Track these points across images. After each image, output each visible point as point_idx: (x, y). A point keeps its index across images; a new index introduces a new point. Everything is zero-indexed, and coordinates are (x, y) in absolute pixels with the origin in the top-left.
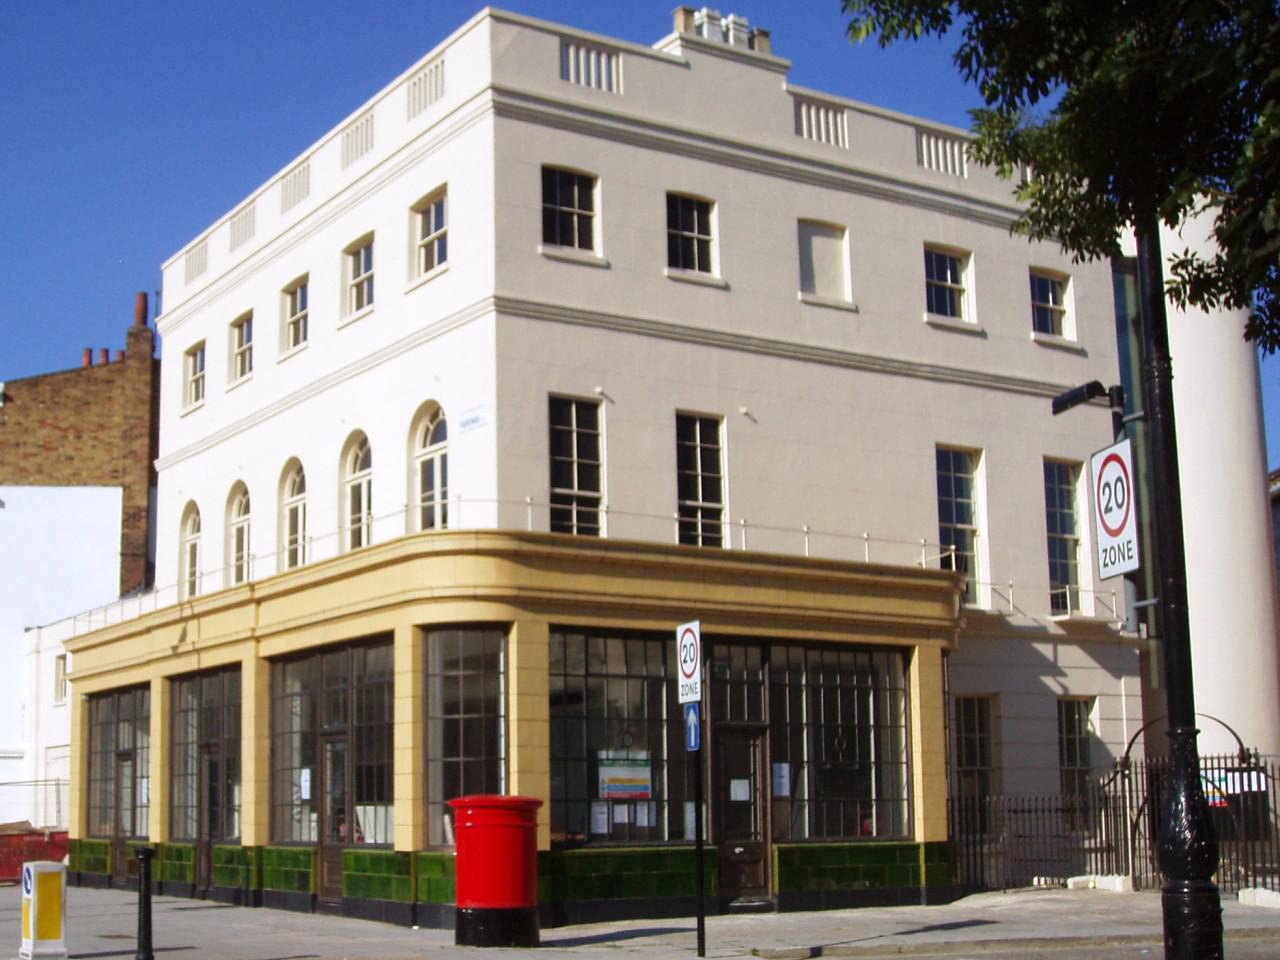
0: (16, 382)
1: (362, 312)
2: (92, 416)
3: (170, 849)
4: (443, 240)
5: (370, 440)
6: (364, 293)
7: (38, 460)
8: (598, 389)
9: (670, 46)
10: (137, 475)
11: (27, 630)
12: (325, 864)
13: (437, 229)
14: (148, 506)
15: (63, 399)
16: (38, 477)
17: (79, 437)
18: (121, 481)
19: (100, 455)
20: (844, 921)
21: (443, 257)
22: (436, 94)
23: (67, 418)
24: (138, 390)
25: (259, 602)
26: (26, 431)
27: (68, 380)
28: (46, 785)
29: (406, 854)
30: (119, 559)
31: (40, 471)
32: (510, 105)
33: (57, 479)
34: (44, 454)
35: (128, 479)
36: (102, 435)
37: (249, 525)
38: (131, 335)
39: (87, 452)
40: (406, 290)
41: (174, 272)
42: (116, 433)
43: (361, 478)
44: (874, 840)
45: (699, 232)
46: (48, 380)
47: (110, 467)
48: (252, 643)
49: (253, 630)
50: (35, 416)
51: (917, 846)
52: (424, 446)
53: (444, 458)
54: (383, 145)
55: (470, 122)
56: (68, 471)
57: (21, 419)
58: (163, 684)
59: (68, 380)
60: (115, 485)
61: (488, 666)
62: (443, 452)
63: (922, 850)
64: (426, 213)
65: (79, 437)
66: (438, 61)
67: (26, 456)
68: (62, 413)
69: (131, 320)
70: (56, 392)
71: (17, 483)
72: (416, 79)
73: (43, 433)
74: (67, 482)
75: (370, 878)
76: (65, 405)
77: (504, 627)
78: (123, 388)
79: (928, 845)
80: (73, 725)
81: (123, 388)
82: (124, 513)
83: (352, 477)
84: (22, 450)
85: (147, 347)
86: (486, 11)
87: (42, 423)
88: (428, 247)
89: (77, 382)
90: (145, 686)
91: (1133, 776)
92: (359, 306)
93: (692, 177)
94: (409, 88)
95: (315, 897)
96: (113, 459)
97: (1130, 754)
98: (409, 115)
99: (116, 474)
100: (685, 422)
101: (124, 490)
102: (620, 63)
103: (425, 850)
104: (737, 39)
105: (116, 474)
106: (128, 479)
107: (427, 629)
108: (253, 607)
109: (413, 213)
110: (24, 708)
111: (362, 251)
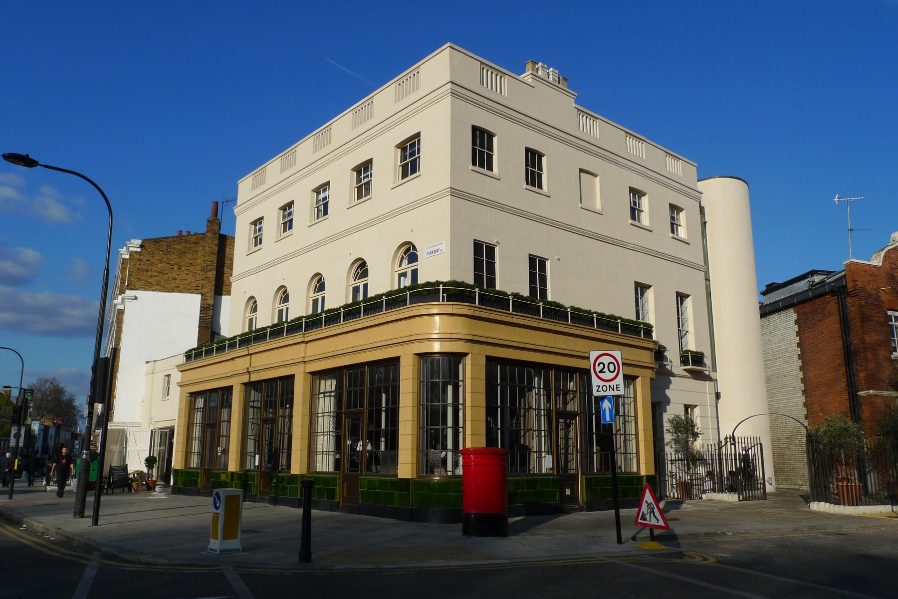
0: (148, 240)
1: (257, 248)
2: (187, 259)
3: (185, 472)
4: (291, 221)
5: (368, 263)
6: (288, 225)
7: (158, 279)
8: (496, 241)
9: (527, 77)
10: (210, 288)
11: (147, 362)
12: (262, 480)
13: (418, 154)
14: (214, 304)
15: (172, 250)
16: (157, 287)
17: (179, 269)
18: (200, 291)
19: (190, 278)
20: (593, 513)
21: (291, 228)
22: (285, 168)
23: (174, 259)
24: (212, 248)
25: (307, 342)
26: (152, 264)
27: (175, 241)
28: (323, 432)
29: (407, 480)
30: (197, 329)
31: (158, 284)
32: (458, 91)
33: (168, 289)
34: (161, 276)
35: (205, 290)
36: (191, 268)
37: (256, 317)
38: (209, 221)
39: (183, 277)
40: (392, 188)
41: (245, 187)
42: (199, 268)
43: (253, 315)
44: (595, 474)
45: (538, 170)
46: (164, 240)
47: (194, 284)
48: (302, 365)
49: (248, 368)
50: (157, 257)
51: (642, 477)
52: (251, 313)
53: (287, 309)
54: (270, 182)
55: (436, 101)
56: (172, 285)
57: (150, 258)
58: (241, 388)
59: (175, 241)
60: (197, 293)
61: (454, 378)
62: (287, 306)
63: (645, 478)
64: (404, 150)
65: (179, 269)
66: (329, 128)
67: (151, 277)
68: (172, 257)
69: (209, 214)
70: (169, 246)
71: (146, 290)
72: (256, 175)
73: (160, 265)
74: (172, 290)
75: (379, 493)
76: (173, 253)
77: (461, 356)
78: (204, 247)
79: (647, 476)
80: (180, 409)
81: (204, 247)
82: (201, 307)
83: (249, 315)
84: (149, 273)
85: (217, 228)
86: (448, 44)
87: (161, 261)
88: (285, 223)
89: (180, 242)
90: (229, 389)
91: (737, 444)
92: (256, 245)
93: (538, 143)
94: (253, 178)
95: (200, 490)
96: (196, 280)
97: (734, 434)
98: (314, 151)
99: (198, 288)
100: (532, 259)
101: (202, 296)
102: (505, 80)
103: (308, 473)
104: (554, 79)
105: (198, 288)
106: (205, 290)
107: (421, 355)
108: (304, 344)
109: (397, 148)
110: (143, 402)
111: (364, 168)
